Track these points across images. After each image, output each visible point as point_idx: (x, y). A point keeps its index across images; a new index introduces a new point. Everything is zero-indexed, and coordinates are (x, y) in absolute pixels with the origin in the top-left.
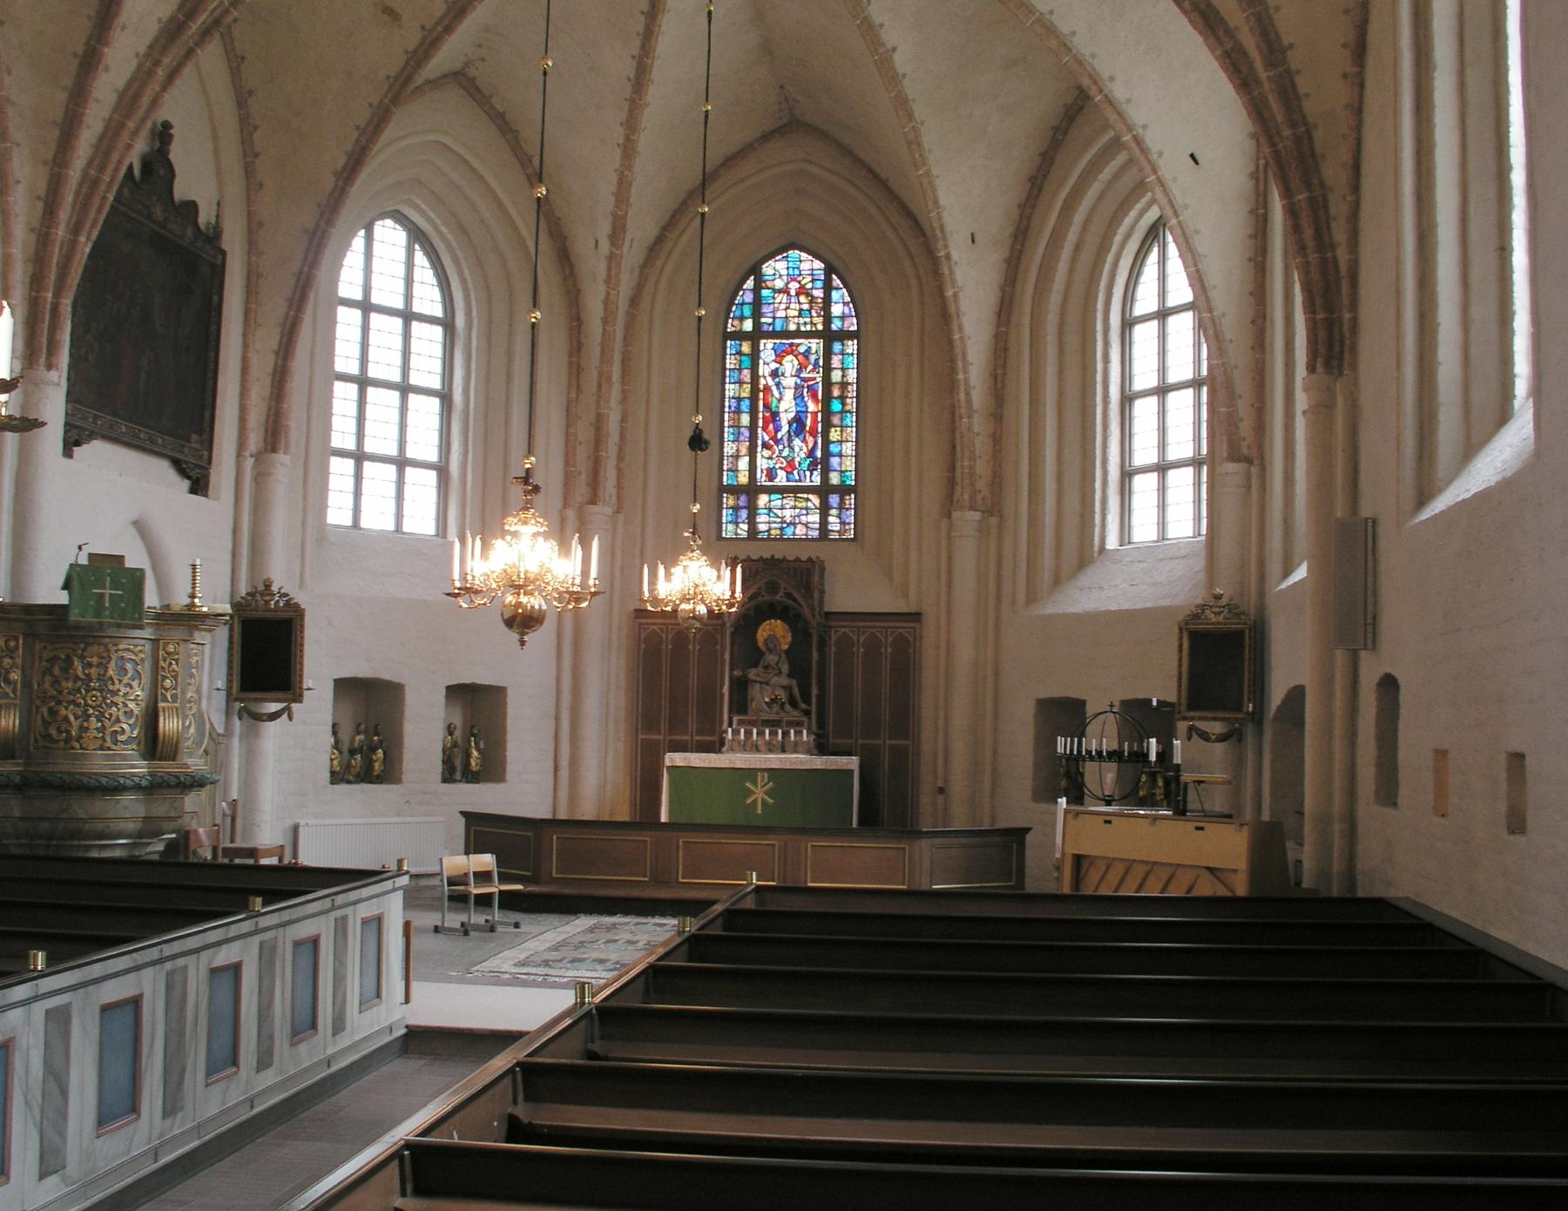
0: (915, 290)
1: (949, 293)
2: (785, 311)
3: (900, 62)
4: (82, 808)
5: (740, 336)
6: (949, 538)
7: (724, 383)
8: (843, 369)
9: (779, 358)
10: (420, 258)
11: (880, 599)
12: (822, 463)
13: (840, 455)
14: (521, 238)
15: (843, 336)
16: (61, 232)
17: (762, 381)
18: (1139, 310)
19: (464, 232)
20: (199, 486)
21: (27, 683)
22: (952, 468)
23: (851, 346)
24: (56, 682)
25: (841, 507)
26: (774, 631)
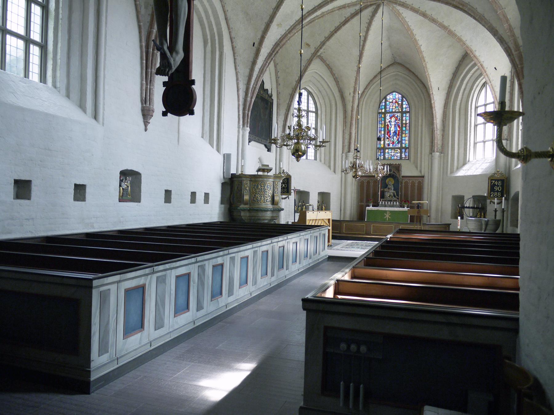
0: (424, 102)
1: (433, 102)
2: (391, 107)
4: (260, 214)
5: (382, 113)
9: (391, 118)
11: (415, 173)
12: (400, 142)
15: (406, 112)
16: (249, 99)
18: (479, 105)
21: (250, 190)
25: (405, 152)
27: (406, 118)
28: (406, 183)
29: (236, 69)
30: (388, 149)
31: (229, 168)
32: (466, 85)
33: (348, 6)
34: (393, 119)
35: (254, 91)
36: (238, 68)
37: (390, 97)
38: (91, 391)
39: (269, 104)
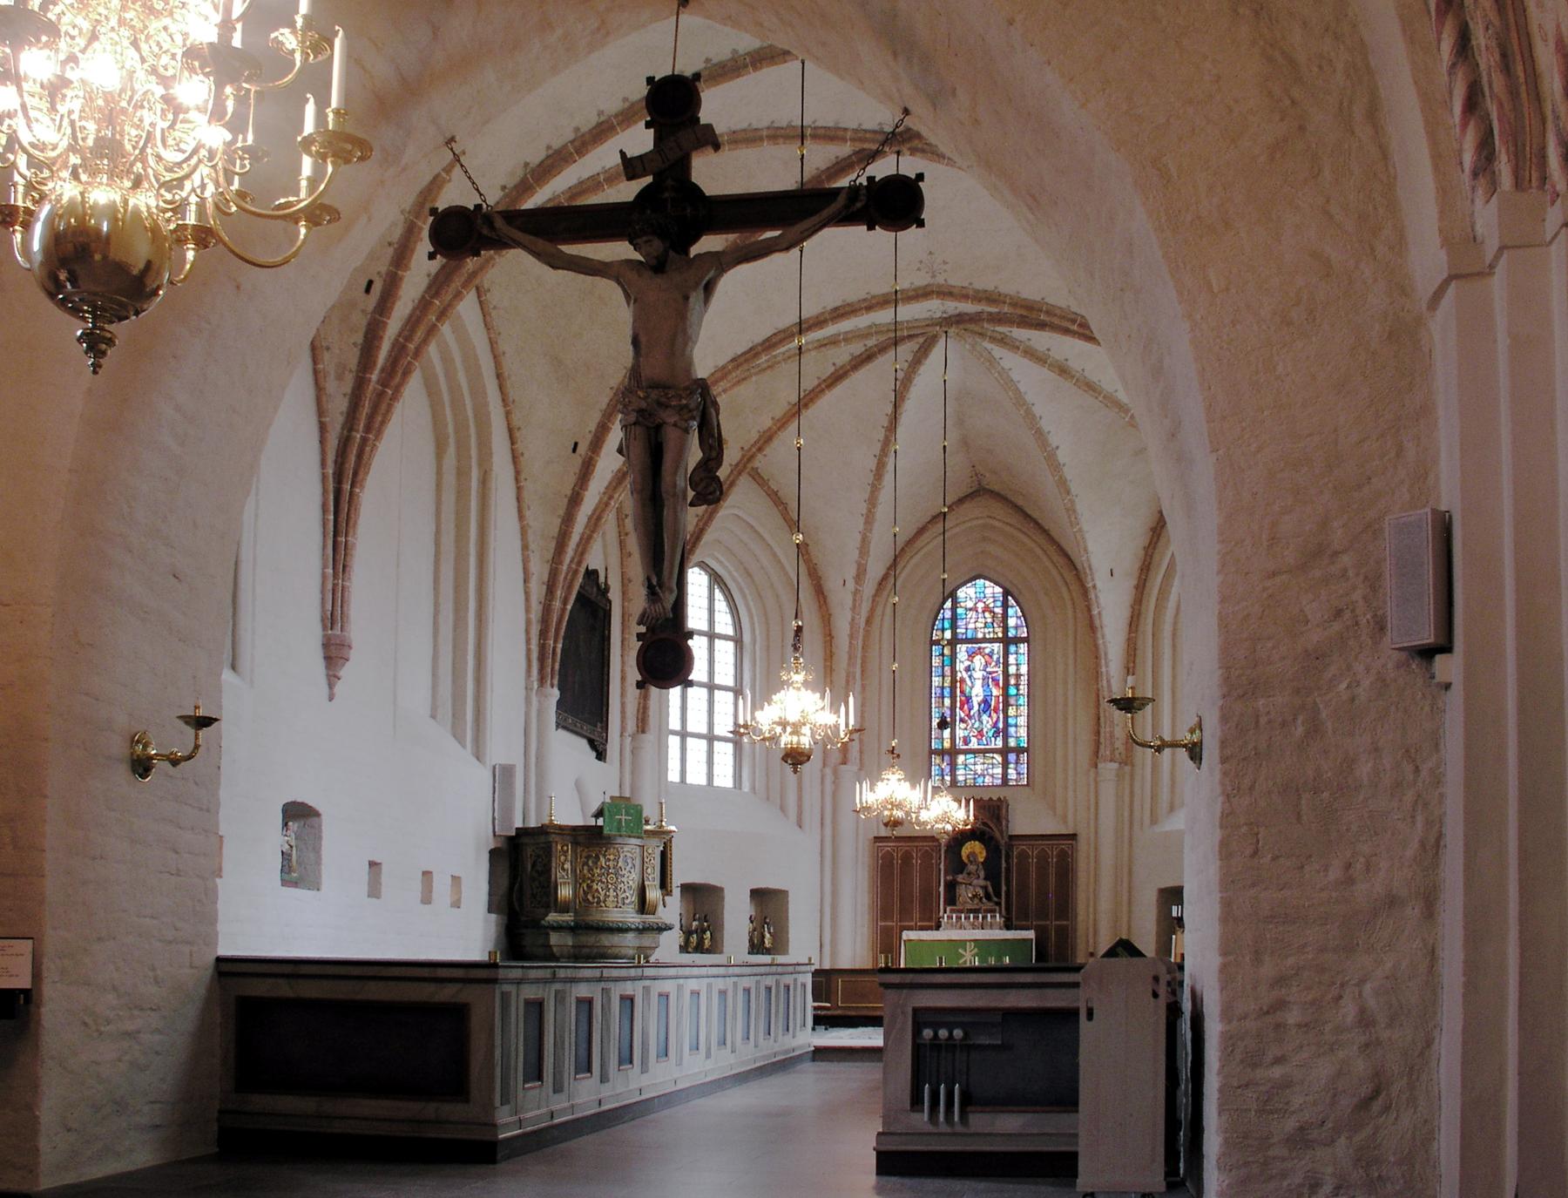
1: (1095, 612)
2: (974, 624)
3: (1062, 456)
6: (1096, 782)
9: (971, 656)
10: (718, 595)
14: (786, 574)
15: (1017, 640)
16: (557, 604)
19: (750, 575)
20: (601, 756)
21: (574, 871)
22: (1098, 733)
23: (1023, 648)
24: (590, 870)
26: (973, 848)
27: (1020, 660)
28: (1023, 856)
29: (521, 517)
30: (966, 752)
31: (507, 810)
33: (845, 340)
34: (978, 661)
35: (572, 581)
36: (527, 513)
37: (967, 593)
38: (499, 1156)
39: (601, 614)
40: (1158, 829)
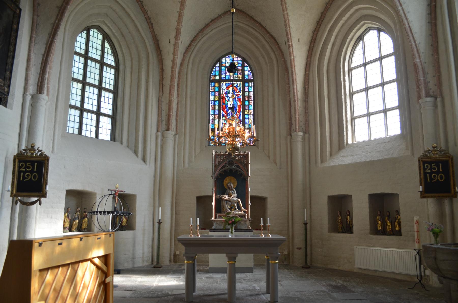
1: (292, 58)
5: (215, 81)
6: (291, 142)
7: (210, 96)
8: (249, 92)
10: (106, 45)
13: (248, 119)
15: (248, 81)
17: (222, 95)
18: (353, 65)
23: (251, 84)
27: (249, 89)
32: (336, 38)
40: (326, 165)
